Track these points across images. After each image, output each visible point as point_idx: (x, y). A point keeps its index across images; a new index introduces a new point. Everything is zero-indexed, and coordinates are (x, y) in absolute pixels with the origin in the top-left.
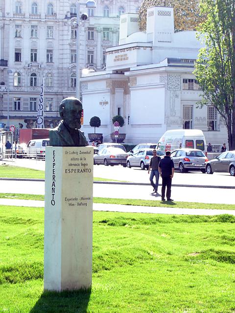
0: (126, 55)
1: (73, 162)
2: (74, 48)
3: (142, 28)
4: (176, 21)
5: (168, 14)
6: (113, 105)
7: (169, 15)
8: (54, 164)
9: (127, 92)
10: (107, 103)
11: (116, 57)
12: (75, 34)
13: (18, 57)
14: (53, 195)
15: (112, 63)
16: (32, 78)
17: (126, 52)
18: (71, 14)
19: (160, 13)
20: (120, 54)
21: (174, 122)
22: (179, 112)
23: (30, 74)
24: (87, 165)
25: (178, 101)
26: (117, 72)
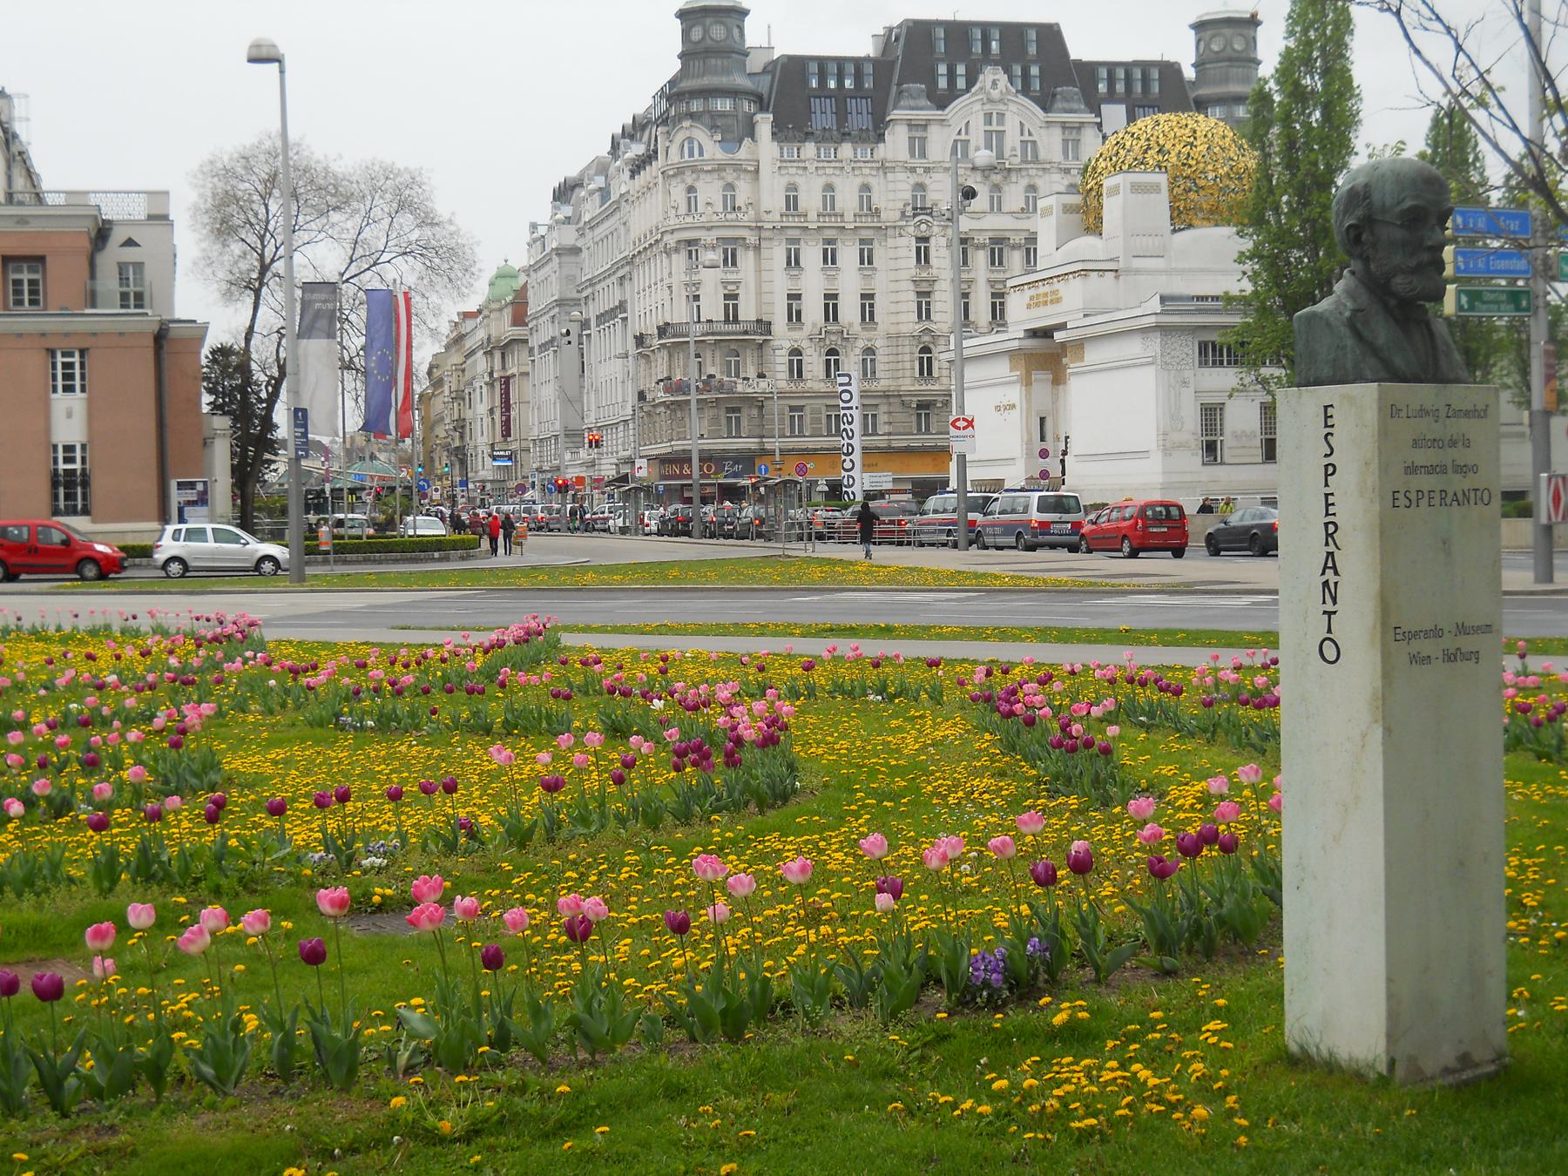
0: (1055, 292)
1: (1422, 457)
2: (924, 287)
3: (1094, 226)
4: (1174, 199)
5: (1155, 188)
6: (1029, 410)
7: (1159, 192)
8: (1330, 470)
9: (1058, 380)
10: (1014, 406)
11: (1031, 298)
12: (923, 256)
13: (795, 316)
14: (1329, 614)
15: (1022, 314)
16: (828, 361)
17: (1056, 285)
18: (915, 209)
19: (1137, 188)
20: (1043, 289)
21: (1180, 446)
22: (1192, 421)
23: (824, 351)
24: (1474, 469)
25: (1188, 395)
26: (1034, 333)
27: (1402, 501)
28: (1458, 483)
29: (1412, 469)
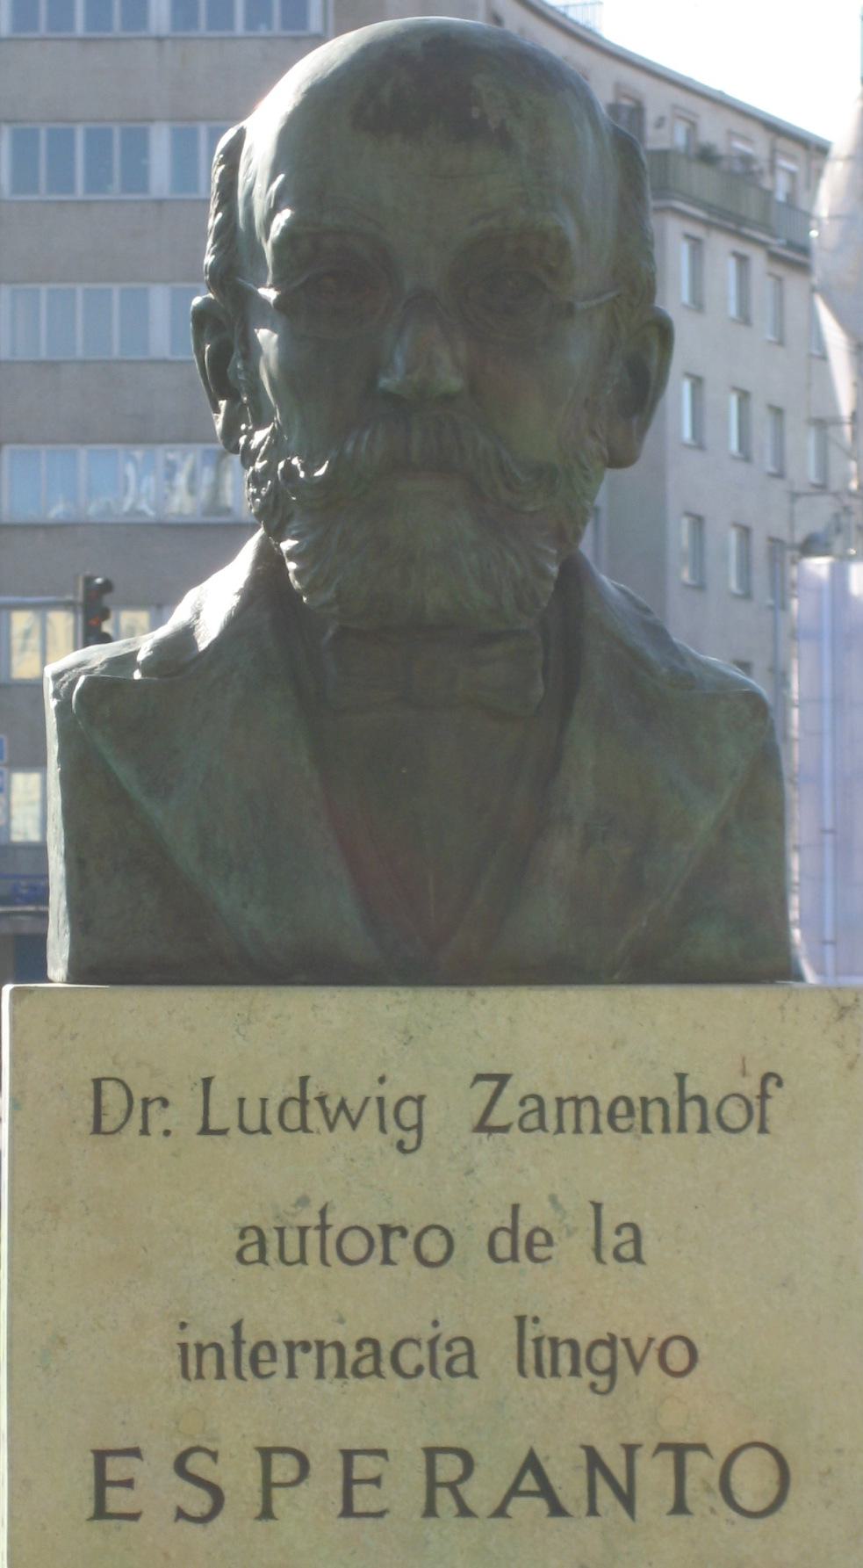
1: (284, 1304)
24: (680, 1355)
29: (245, 1356)
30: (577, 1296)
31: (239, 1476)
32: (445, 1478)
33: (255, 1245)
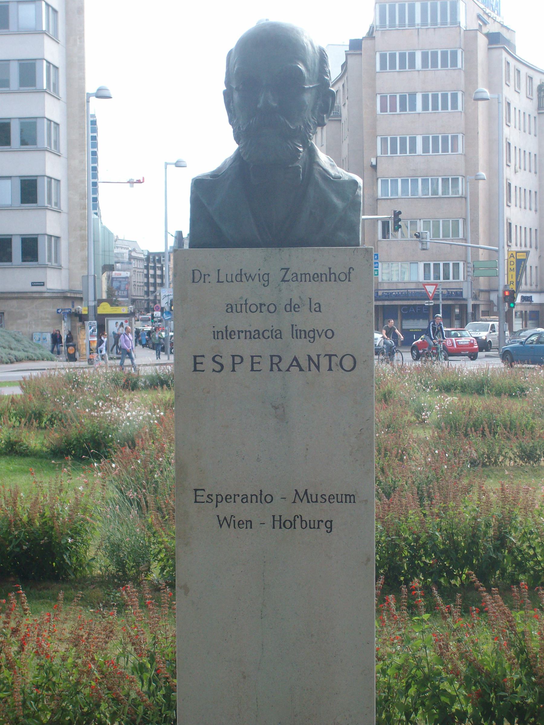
1: (238, 322)
24: (329, 334)
27: (208, 364)
28: (301, 349)
29: (228, 334)
30: (305, 320)
31: (227, 362)
32: (275, 362)
33: (230, 308)
